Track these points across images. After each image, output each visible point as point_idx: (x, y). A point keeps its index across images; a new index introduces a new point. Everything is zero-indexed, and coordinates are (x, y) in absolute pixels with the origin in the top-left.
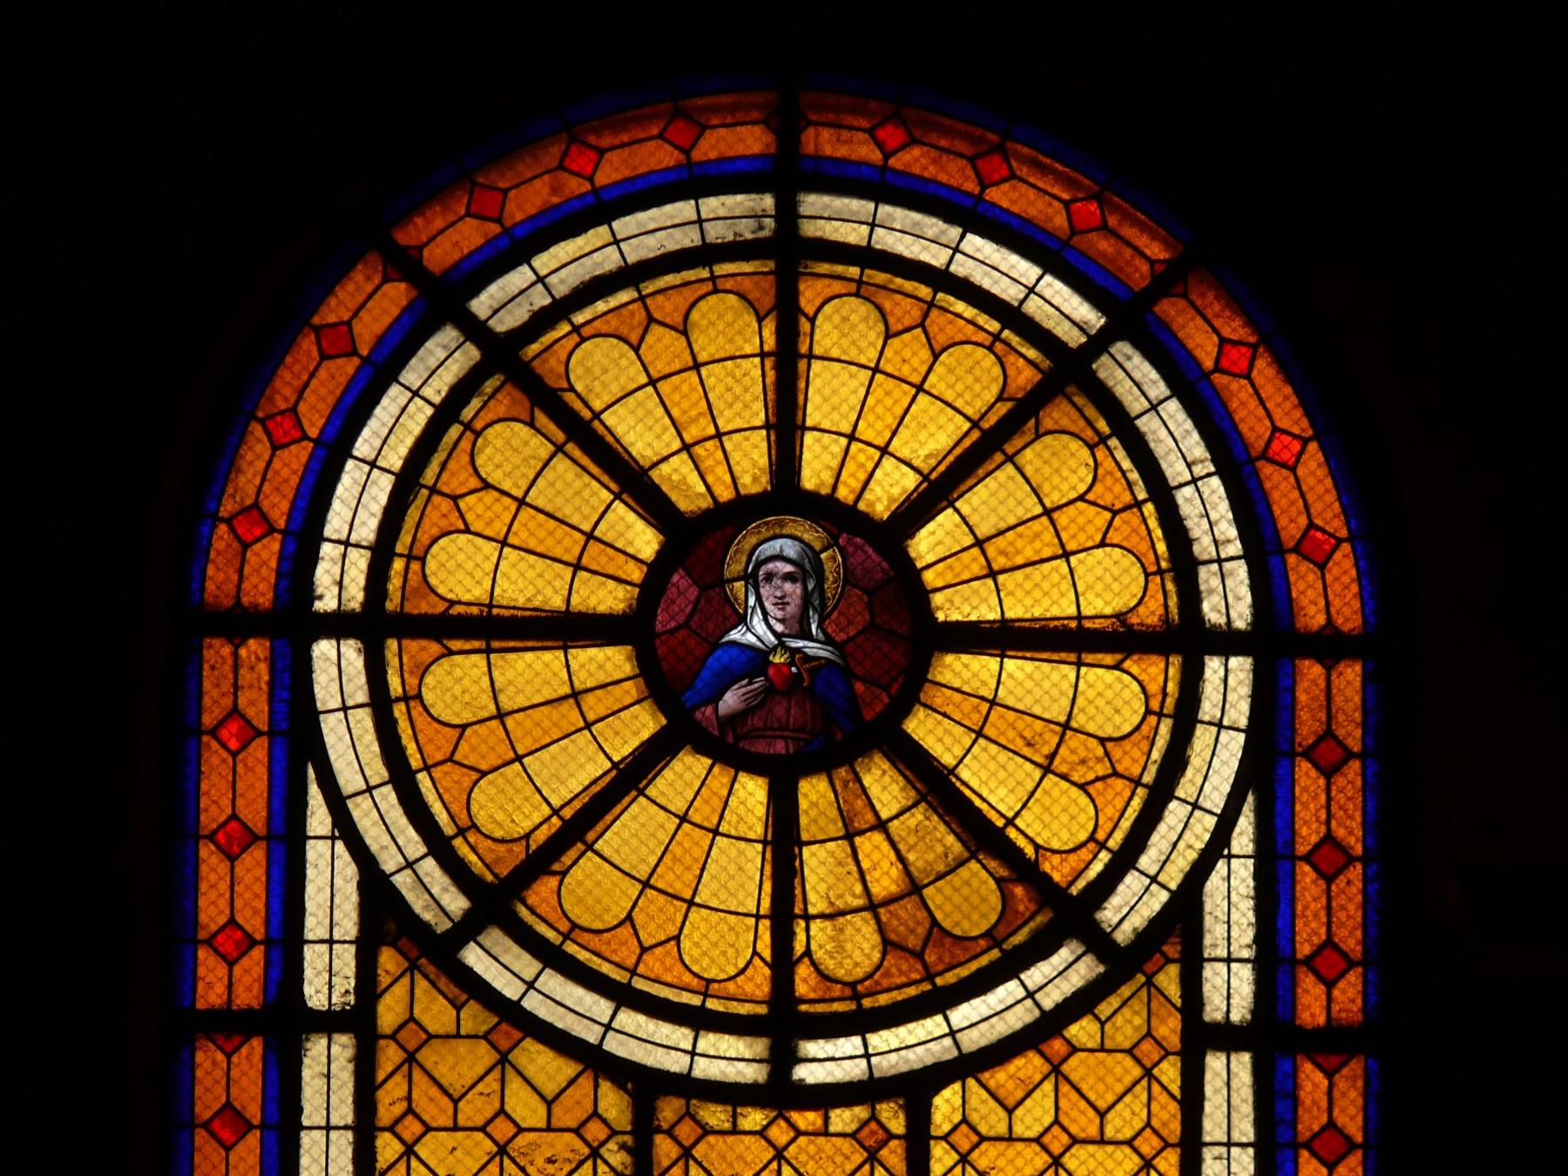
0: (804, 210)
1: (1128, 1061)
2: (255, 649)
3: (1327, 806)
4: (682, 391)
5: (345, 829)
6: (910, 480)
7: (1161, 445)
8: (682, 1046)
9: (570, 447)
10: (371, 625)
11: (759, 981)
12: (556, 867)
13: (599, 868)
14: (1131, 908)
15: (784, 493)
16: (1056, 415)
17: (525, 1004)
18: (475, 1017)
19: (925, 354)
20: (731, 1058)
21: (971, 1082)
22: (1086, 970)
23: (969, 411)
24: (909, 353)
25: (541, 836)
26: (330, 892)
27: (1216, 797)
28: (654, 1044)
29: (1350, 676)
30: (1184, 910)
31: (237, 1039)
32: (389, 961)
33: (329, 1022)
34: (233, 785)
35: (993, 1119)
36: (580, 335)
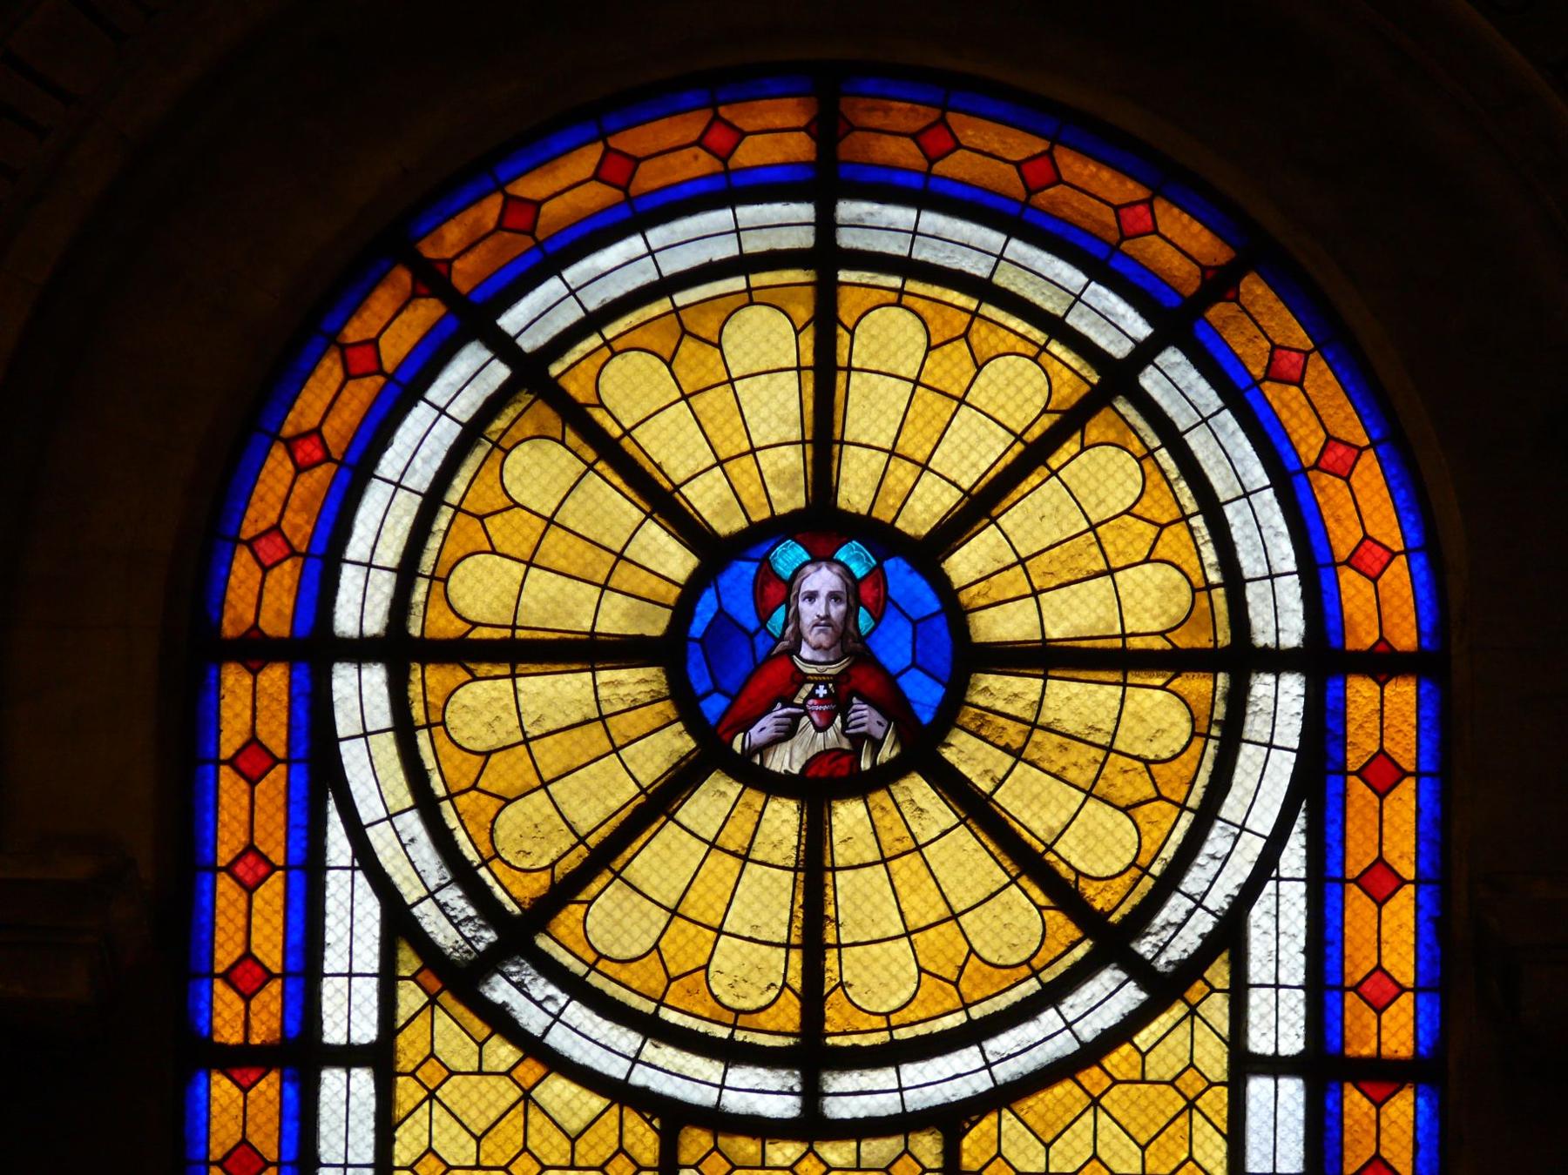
0: (794, 1101)
1: (1172, 1093)
2: (275, 678)
3: (1390, 827)
4: (924, 907)
5: (365, 857)
6: (950, 498)
7: (425, 853)
8: (712, 1081)
9: (600, 466)
10: (397, 650)
11: (789, 1014)
12: (581, 897)
13: (1010, 416)
14: (1178, 933)
15: (821, 522)
16: (536, 886)
17: (1083, 279)
18: (502, 1053)
19: (968, 364)
20: (766, 1093)
21: (1005, 1112)
22: (1132, 996)
23: (1012, 425)
24: (951, 367)
25: (1071, 447)
26: (352, 923)
27: (1265, 819)
28: (686, 1077)
29: (1403, 692)
30: (1230, 934)
31: (253, 1076)
32: (410, 998)
33: (348, 1056)
34: (247, 813)
35: (1031, 1153)
36: (611, 349)
